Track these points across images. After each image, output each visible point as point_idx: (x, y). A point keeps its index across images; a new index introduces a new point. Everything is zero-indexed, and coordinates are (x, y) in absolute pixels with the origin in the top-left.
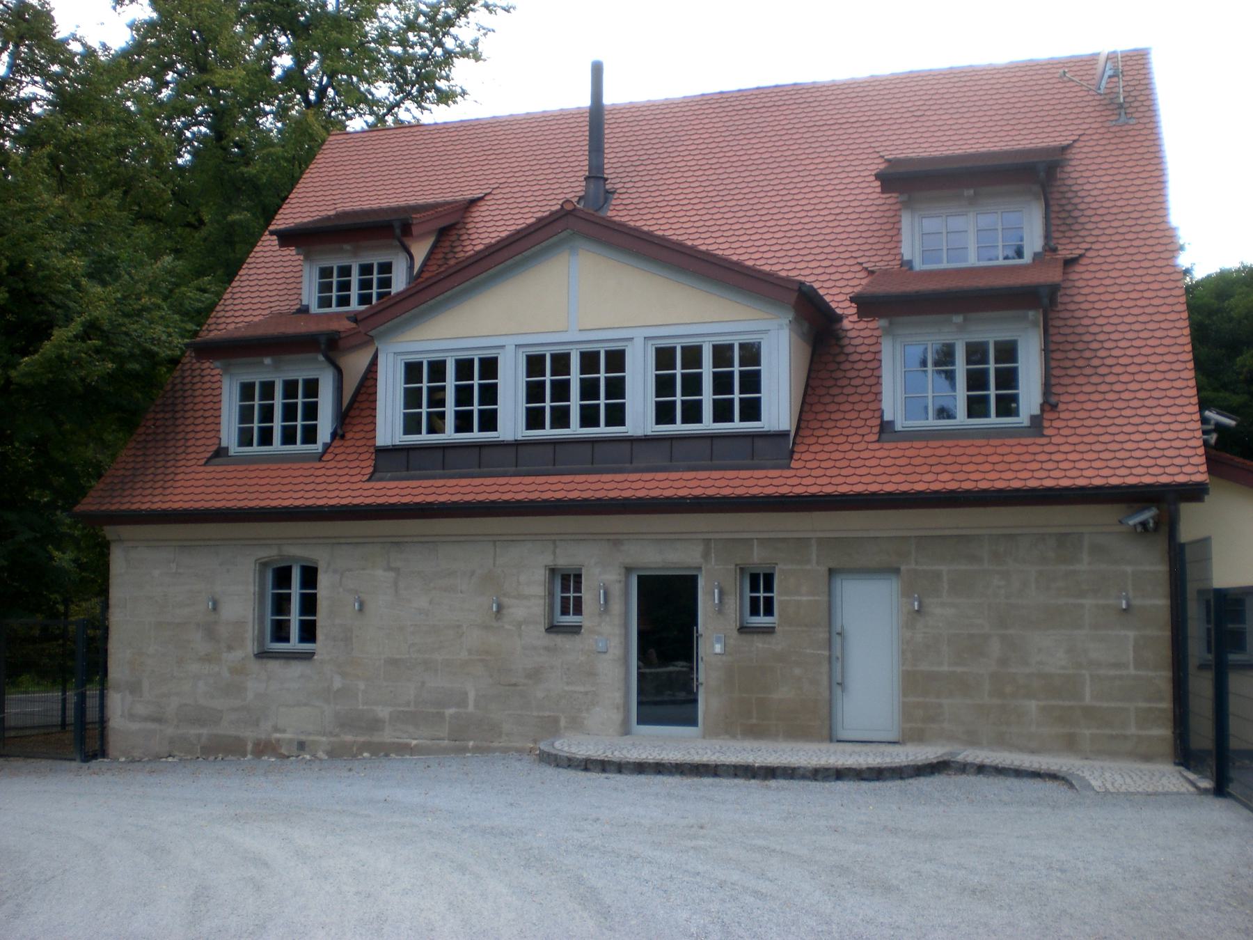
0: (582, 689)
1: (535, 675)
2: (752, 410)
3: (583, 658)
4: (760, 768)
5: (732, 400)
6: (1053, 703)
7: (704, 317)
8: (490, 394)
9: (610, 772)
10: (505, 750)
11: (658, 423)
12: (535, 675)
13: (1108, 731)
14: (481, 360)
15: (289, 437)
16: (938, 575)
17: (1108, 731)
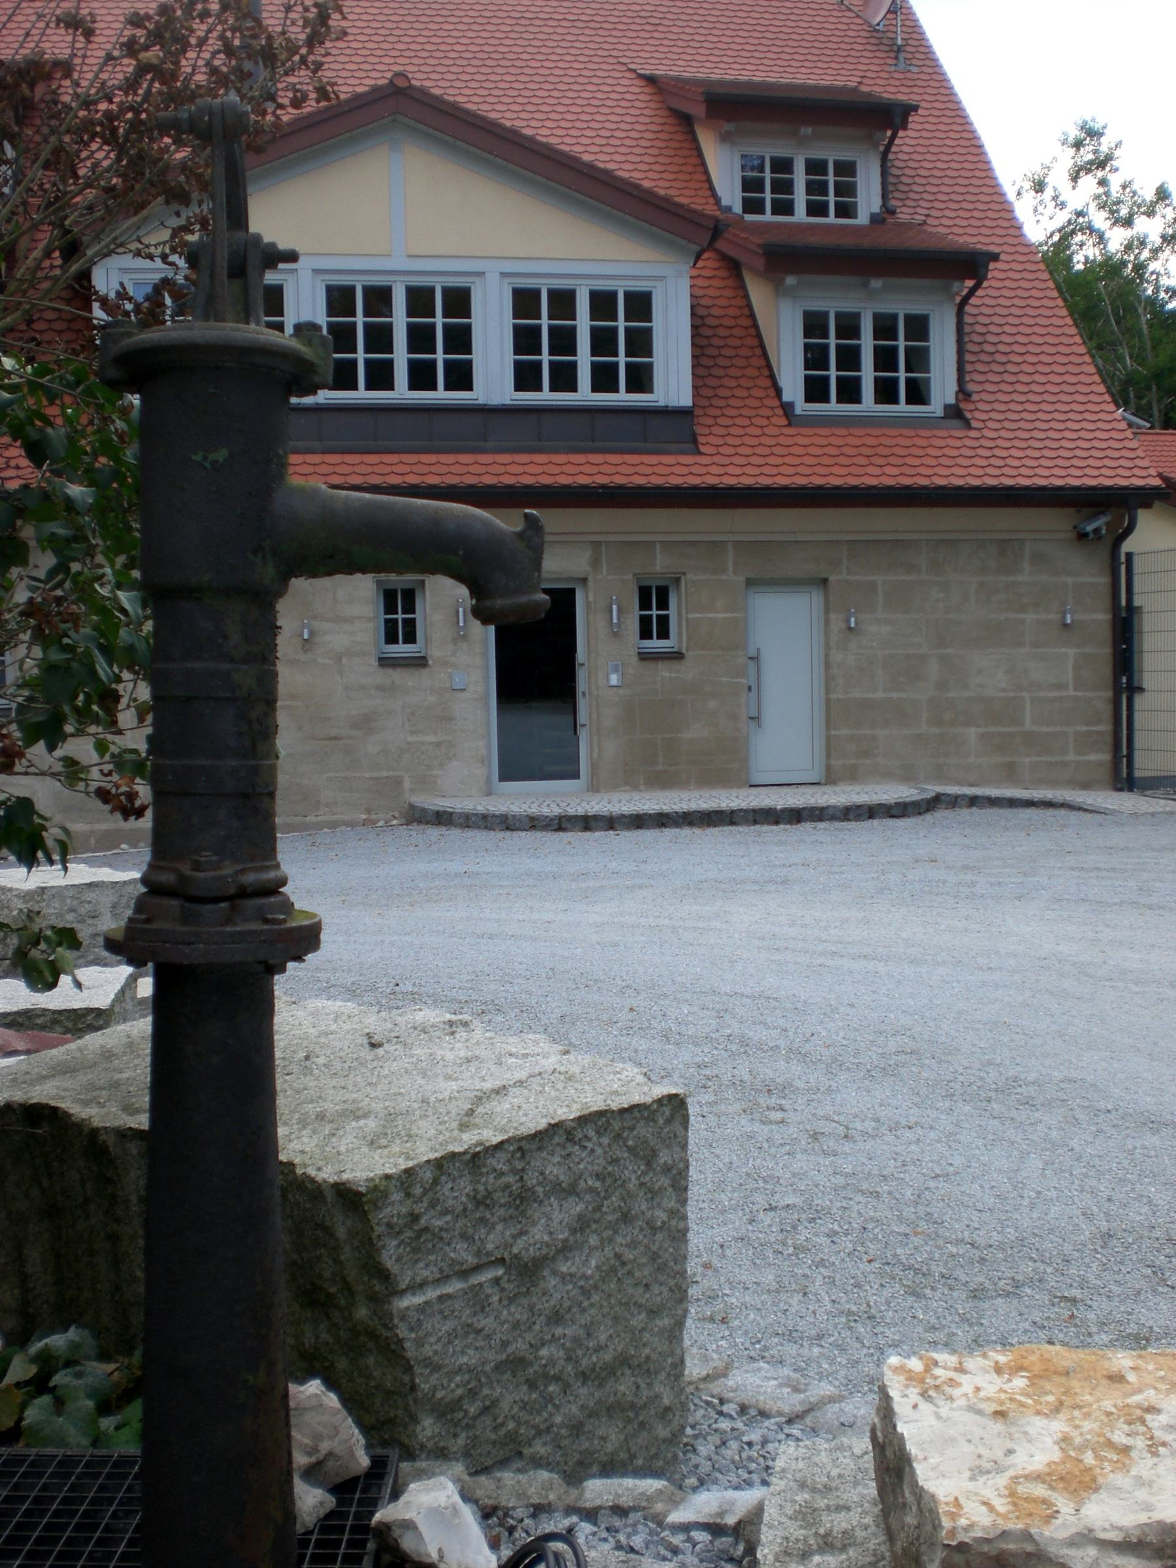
0: (431, 738)
1: (366, 723)
2: (640, 379)
3: (432, 699)
4: (784, 810)
5: (616, 364)
6: (993, 729)
7: (585, 253)
8: (460, 339)
9: (597, 829)
10: (333, 825)
11: (518, 388)
12: (366, 723)
13: (1045, 758)
14: (628, 295)
15: (886, 392)
16: (872, 587)
17: (1045, 758)
